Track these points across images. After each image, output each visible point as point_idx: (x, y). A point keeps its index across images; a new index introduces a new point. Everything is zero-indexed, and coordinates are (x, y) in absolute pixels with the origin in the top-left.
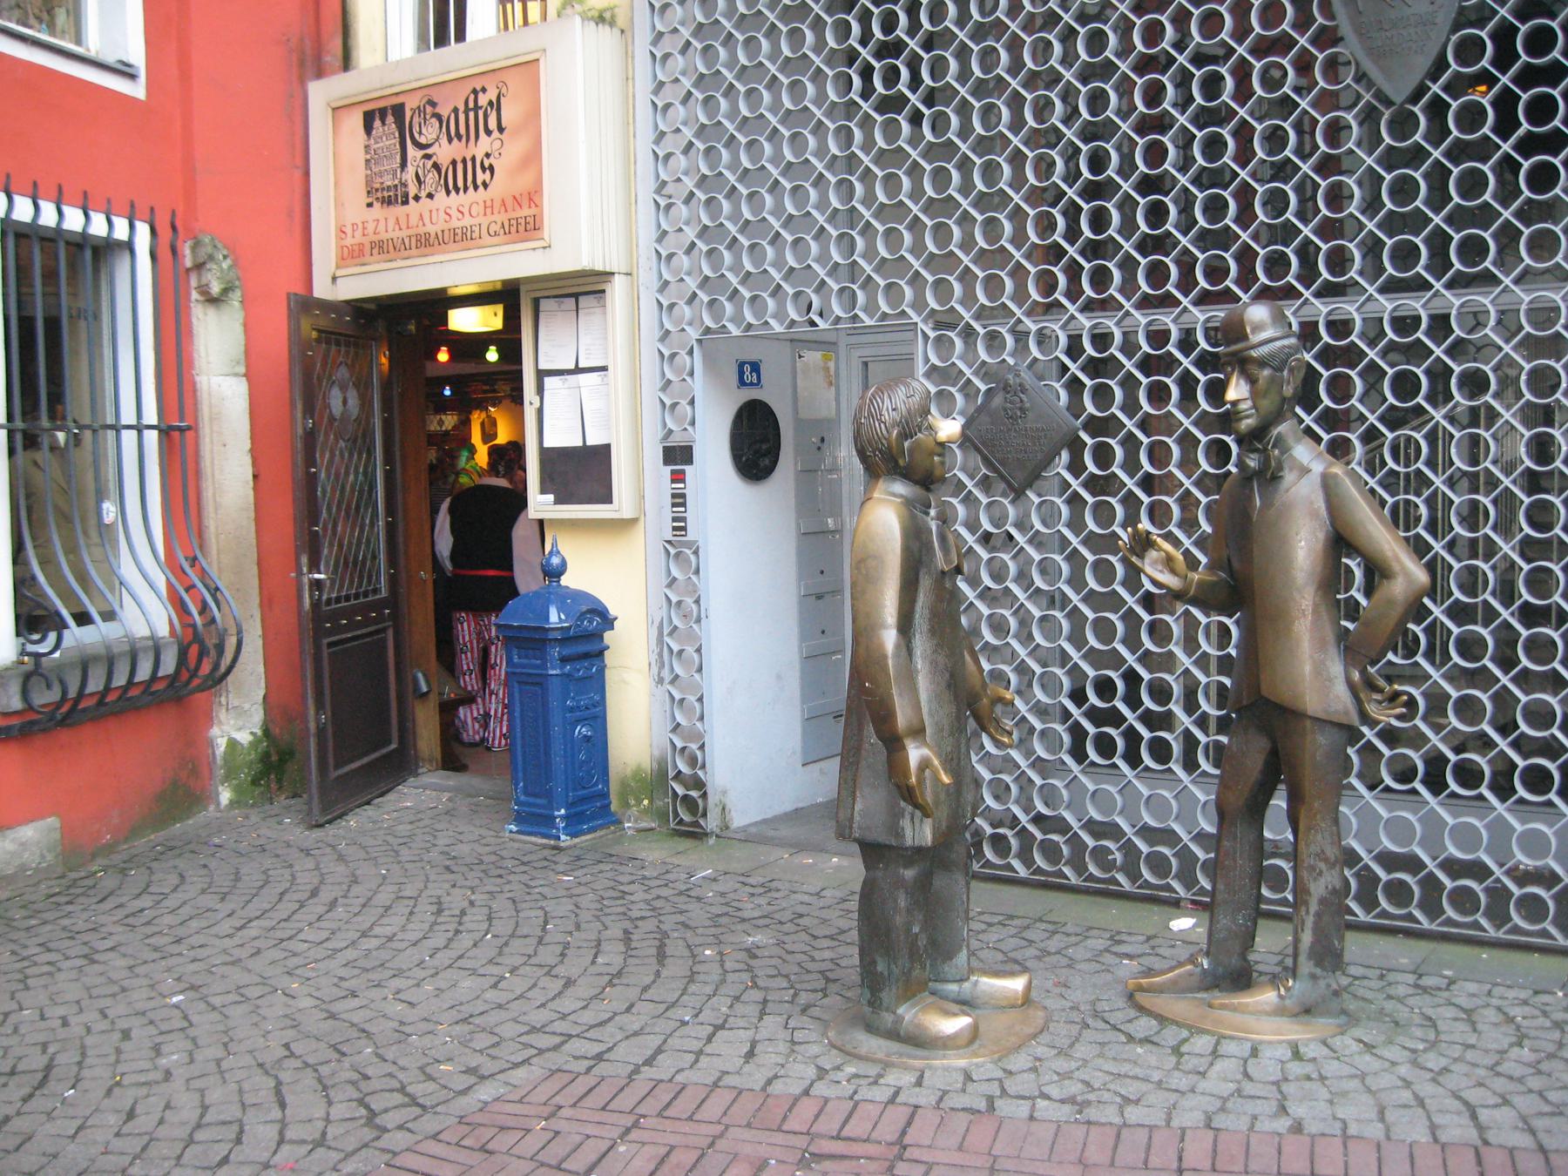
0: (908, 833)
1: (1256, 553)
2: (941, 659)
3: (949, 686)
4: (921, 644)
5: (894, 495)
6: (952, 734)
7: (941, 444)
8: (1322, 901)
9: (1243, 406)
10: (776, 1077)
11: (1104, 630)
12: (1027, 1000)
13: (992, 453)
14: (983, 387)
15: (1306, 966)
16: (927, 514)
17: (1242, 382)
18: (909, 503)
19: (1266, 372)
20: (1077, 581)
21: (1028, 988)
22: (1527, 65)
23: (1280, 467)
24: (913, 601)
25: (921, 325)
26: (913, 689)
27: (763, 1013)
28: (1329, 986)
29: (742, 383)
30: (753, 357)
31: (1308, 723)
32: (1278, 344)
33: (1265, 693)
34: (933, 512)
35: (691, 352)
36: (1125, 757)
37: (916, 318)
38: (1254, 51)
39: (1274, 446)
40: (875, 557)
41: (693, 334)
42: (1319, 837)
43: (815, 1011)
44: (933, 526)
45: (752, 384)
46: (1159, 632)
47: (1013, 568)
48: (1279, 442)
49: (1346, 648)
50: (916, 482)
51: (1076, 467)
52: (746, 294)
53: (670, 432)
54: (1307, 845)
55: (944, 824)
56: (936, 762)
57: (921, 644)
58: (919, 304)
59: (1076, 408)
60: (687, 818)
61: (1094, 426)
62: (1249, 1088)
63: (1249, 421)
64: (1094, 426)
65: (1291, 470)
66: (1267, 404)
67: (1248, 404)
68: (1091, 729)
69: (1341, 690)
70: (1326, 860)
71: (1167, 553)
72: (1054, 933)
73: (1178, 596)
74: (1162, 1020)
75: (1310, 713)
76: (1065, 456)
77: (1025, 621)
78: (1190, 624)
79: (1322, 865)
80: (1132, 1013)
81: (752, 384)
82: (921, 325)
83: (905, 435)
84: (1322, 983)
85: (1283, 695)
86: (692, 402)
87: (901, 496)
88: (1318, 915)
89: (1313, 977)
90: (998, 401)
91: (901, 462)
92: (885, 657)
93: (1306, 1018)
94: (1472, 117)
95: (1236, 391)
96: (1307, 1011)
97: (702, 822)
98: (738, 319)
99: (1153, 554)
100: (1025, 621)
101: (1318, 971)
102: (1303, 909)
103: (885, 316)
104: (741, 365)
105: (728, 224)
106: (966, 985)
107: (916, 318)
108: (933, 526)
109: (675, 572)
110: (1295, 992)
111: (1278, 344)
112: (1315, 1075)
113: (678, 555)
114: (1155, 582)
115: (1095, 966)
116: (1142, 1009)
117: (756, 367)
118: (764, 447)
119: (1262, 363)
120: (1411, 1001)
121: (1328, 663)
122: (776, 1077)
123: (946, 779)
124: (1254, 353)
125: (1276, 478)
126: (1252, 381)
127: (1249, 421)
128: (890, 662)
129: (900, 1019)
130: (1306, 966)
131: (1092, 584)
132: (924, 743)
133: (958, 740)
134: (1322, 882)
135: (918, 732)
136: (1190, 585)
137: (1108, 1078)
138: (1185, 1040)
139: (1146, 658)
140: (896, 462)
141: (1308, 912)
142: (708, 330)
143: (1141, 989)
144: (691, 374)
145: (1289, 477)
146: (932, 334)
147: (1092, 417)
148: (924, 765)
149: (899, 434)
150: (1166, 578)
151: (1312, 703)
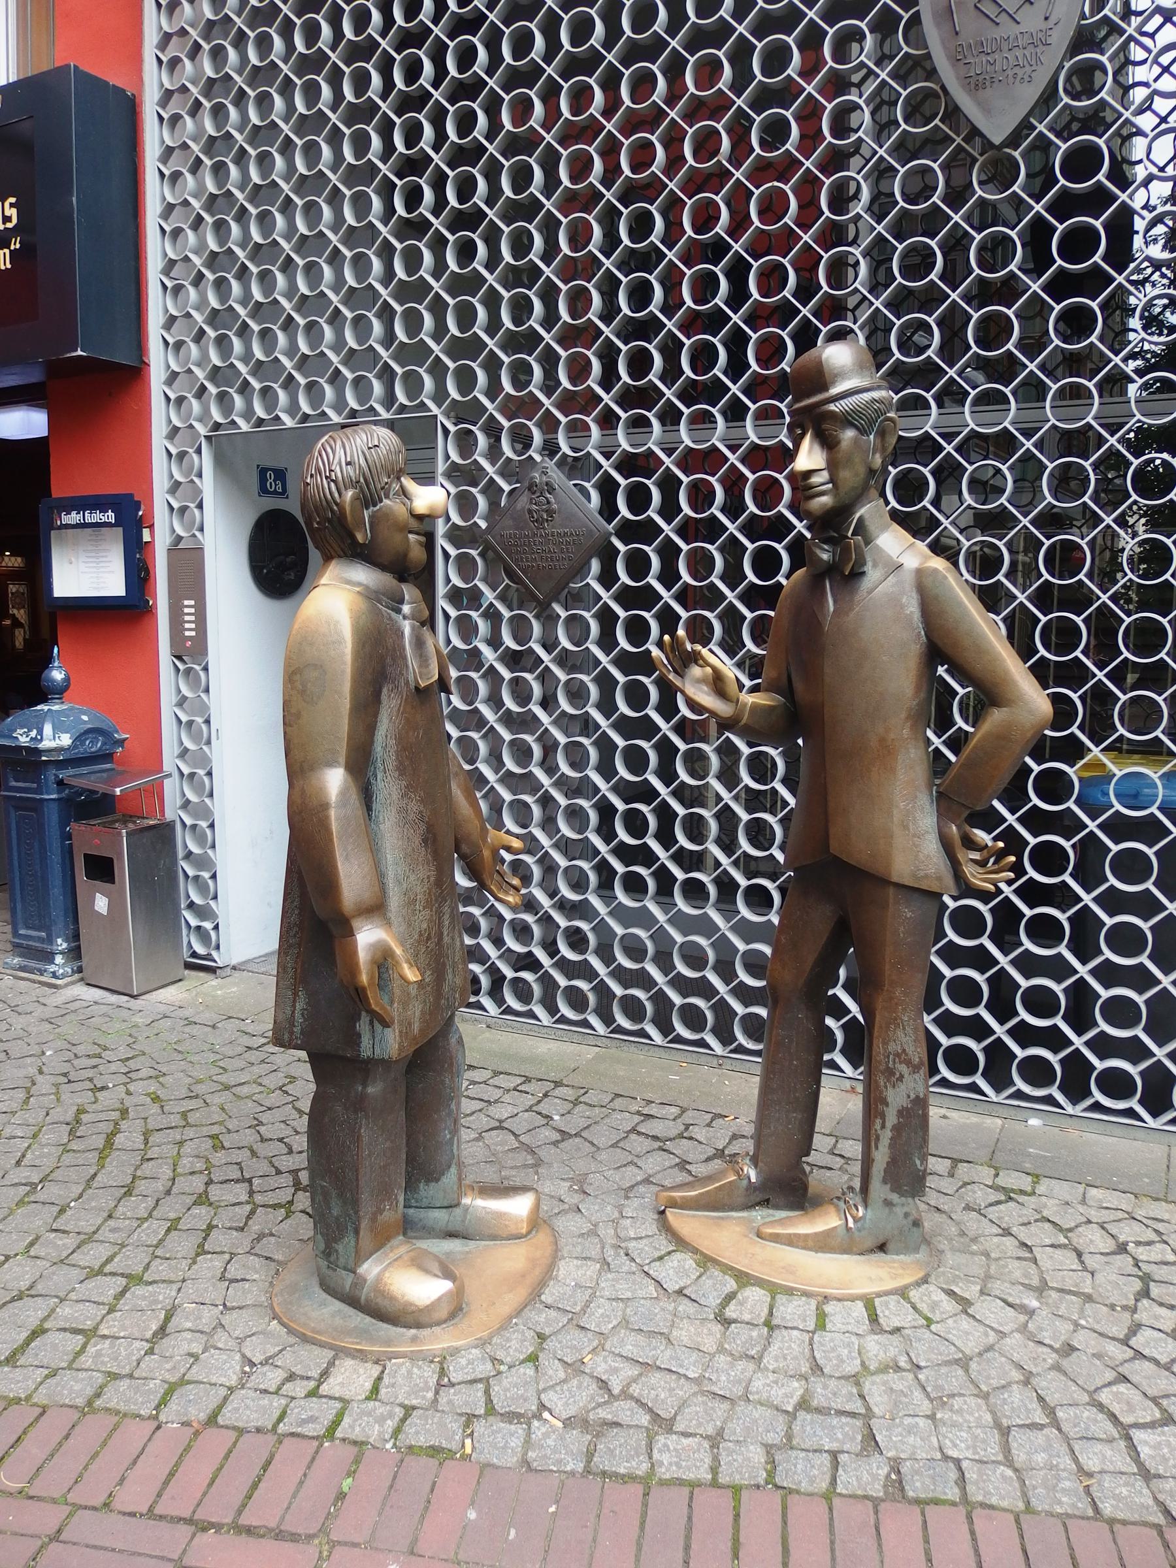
0: (366, 1041)
1: (827, 670)
2: (414, 807)
3: (425, 841)
4: (387, 787)
5: (349, 582)
6: (428, 905)
7: (420, 518)
8: (901, 1113)
9: (815, 480)
10: (183, 1382)
11: (636, 760)
12: (536, 1221)
13: (516, 562)
14: (507, 488)
15: (879, 1189)
16: (399, 611)
17: (817, 448)
18: (372, 596)
19: (849, 434)
20: (607, 706)
21: (537, 1206)
22: (1064, 191)
23: (861, 561)
24: (371, 729)
25: (441, 418)
26: (374, 849)
27: (201, 1251)
28: (906, 1215)
29: (264, 490)
30: (280, 465)
31: (891, 891)
32: (867, 396)
33: (835, 848)
34: (406, 609)
35: (199, 451)
36: (658, 837)
37: (435, 410)
38: (750, 320)
39: (854, 534)
40: (316, 666)
41: (202, 430)
42: (900, 1033)
43: (268, 1246)
44: (407, 627)
45: (275, 492)
46: (696, 762)
47: (537, 690)
48: (861, 528)
49: (940, 795)
50: (383, 567)
51: (608, 578)
52: (256, 385)
53: (179, 539)
54: (885, 1043)
55: (416, 1027)
56: (398, 951)
57: (387, 787)
58: (440, 395)
59: (609, 510)
60: (200, 949)
61: (628, 532)
62: (821, 1394)
63: (824, 499)
64: (628, 532)
65: (875, 566)
66: (850, 477)
67: (824, 476)
68: (620, 868)
69: (931, 847)
70: (908, 1063)
71: (714, 669)
72: (576, 1102)
73: (725, 725)
74: (706, 1261)
75: (895, 878)
76: (595, 566)
77: (550, 748)
78: (728, 752)
79: (903, 1069)
80: (664, 1245)
81: (275, 492)
82: (441, 418)
83: (368, 498)
84: (900, 1211)
85: (858, 852)
86: (200, 506)
87: (359, 584)
88: (897, 1129)
89: (888, 1203)
90: (523, 502)
91: (360, 538)
92: (325, 806)
93: (881, 1256)
94: (997, 250)
95: (809, 457)
96: (882, 1248)
97: (215, 954)
98: (248, 413)
99: (696, 671)
100: (550, 748)
101: (895, 1197)
102: (878, 1121)
103: (306, 418)
104: (263, 472)
105: (284, 360)
106: (457, 1211)
107: (435, 410)
108: (407, 627)
109: (185, 691)
110: (868, 1224)
111: (867, 396)
112: (903, 1362)
113: (188, 671)
114: (693, 705)
115: (621, 1156)
116: (681, 1243)
117: (280, 475)
118: (290, 559)
119: (846, 419)
120: (993, 1212)
121: (918, 815)
122: (183, 1382)
123: (412, 975)
124: (832, 407)
125: (857, 574)
126: (827, 442)
127: (824, 499)
128: (333, 813)
129: (360, 1282)
130: (879, 1189)
131: (624, 708)
132: (388, 923)
133: (440, 914)
134: (902, 1088)
135: (376, 909)
136: (742, 711)
137: (637, 1118)
138: (730, 1297)
139: (681, 793)
140: (353, 537)
141: (883, 1127)
142: (217, 426)
143: (673, 1204)
144: (200, 475)
145: (872, 574)
146: (452, 429)
147: (626, 521)
148: (383, 960)
149: (355, 498)
150: (706, 698)
151: (902, 869)
